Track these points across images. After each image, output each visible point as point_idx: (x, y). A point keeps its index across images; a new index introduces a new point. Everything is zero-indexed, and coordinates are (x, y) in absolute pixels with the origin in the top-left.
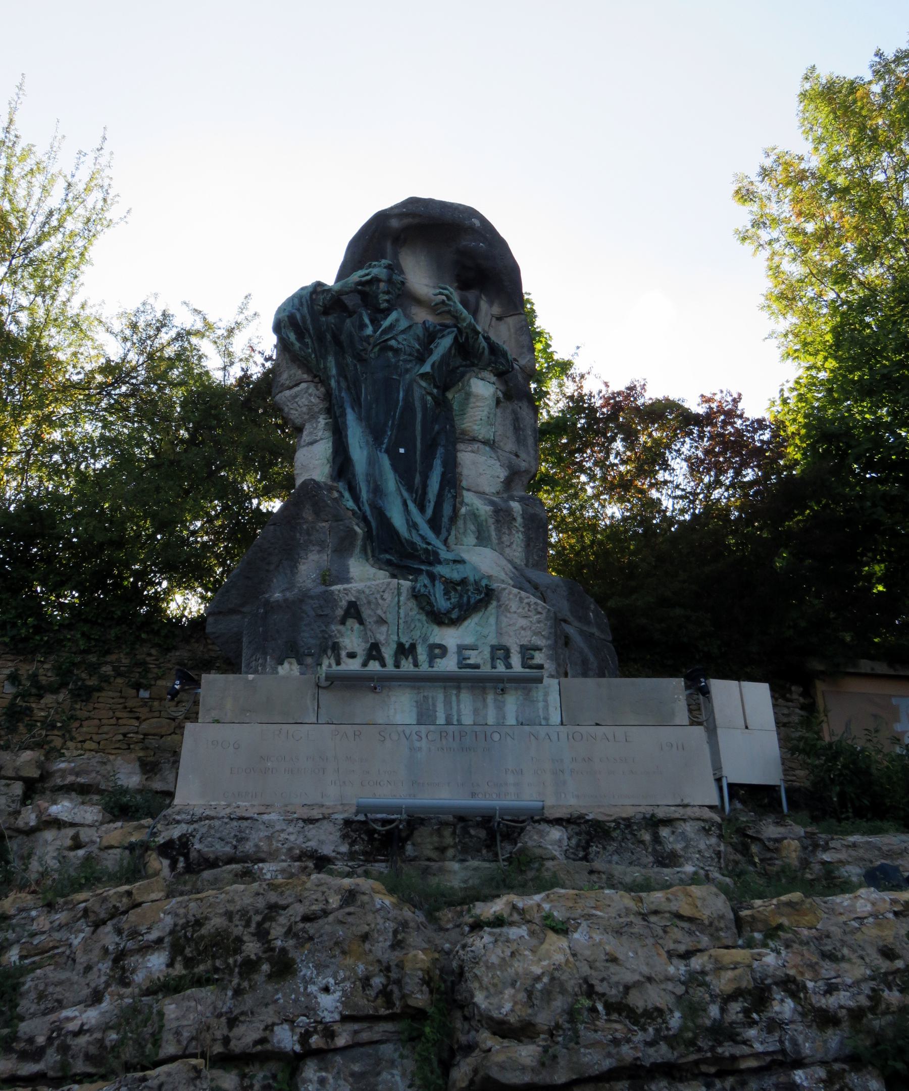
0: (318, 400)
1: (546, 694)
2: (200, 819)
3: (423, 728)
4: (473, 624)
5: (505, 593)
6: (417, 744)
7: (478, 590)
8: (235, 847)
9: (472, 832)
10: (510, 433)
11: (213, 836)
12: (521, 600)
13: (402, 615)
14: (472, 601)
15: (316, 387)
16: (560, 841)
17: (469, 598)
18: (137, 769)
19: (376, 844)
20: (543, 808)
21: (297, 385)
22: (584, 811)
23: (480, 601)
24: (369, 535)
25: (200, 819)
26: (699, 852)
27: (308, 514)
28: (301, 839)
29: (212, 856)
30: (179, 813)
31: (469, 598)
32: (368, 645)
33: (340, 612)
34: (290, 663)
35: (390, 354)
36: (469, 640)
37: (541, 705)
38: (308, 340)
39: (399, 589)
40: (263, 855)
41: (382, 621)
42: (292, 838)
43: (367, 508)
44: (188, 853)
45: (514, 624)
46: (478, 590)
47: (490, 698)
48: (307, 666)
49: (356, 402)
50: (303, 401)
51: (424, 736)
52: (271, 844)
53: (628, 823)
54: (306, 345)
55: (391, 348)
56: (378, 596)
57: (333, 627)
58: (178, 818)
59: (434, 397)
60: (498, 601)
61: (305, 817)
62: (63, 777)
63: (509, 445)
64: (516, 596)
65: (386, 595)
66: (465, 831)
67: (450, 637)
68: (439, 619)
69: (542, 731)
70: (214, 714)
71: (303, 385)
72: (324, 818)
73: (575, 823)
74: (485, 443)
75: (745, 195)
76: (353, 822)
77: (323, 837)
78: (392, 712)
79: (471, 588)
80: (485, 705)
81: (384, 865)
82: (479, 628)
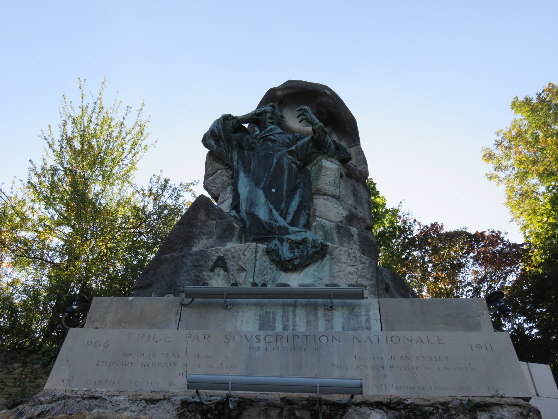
0: (227, 178)
1: (368, 310)
2: (59, 399)
3: (262, 333)
4: (311, 271)
5: (337, 251)
6: (256, 345)
9: (298, 413)
10: (351, 195)
12: (349, 254)
13: (258, 265)
14: (310, 252)
17: (308, 251)
20: (361, 386)
21: (216, 172)
23: (317, 253)
24: (244, 228)
25: (59, 399)
27: (202, 216)
33: (211, 263)
37: (364, 318)
39: (256, 249)
43: (244, 215)
45: (344, 270)
47: (321, 313)
49: (247, 171)
51: (262, 339)
54: (221, 146)
55: (270, 140)
56: (241, 253)
57: (205, 273)
59: (297, 166)
60: (332, 255)
61: (148, 398)
63: (351, 201)
64: (345, 252)
65: (246, 253)
68: (286, 266)
69: (364, 335)
71: (219, 171)
72: (164, 399)
73: (393, 409)
74: (333, 196)
75: (489, 157)
76: (190, 403)
78: (239, 323)
79: (310, 245)
80: (317, 319)
82: (316, 273)
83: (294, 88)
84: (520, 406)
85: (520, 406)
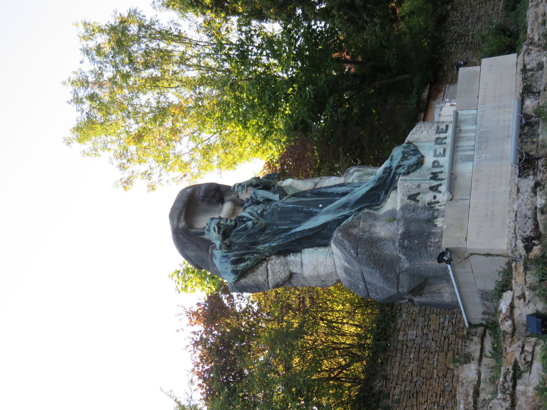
1: (463, 115)
2: (515, 234)
7: (408, 147)
8: (529, 218)
9: (526, 131)
11: (524, 227)
13: (417, 178)
15: (271, 260)
16: (531, 101)
18: (468, 365)
19: (530, 166)
22: (518, 94)
24: (369, 207)
25: (515, 234)
26: (538, 56)
28: (527, 193)
29: (533, 227)
30: (511, 245)
31: (412, 150)
32: (430, 191)
33: (413, 203)
34: (437, 222)
35: (265, 213)
36: (432, 153)
38: (246, 257)
40: (533, 207)
41: (419, 186)
42: (526, 196)
43: (353, 210)
44: (531, 237)
46: (408, 147)
47: (462, 135)
48: (438, 215)
50: (277, 267)
52: (529, 204)
53: (524, 79)
54: (248, 259)
55: (262, 212)
58: (514, 245)
62: (469, 403)
66: (525, 134)
67: (429, 160)
68: (420, 163)
70: (462, 240)
71: (269, 266)
75: (127, 183)
77: (526, 185)
79: (407, 150)
80: (467, 137)
81: (539, 162)
83: (180, 215)
84: (524, 54)
85: (524, 54)
